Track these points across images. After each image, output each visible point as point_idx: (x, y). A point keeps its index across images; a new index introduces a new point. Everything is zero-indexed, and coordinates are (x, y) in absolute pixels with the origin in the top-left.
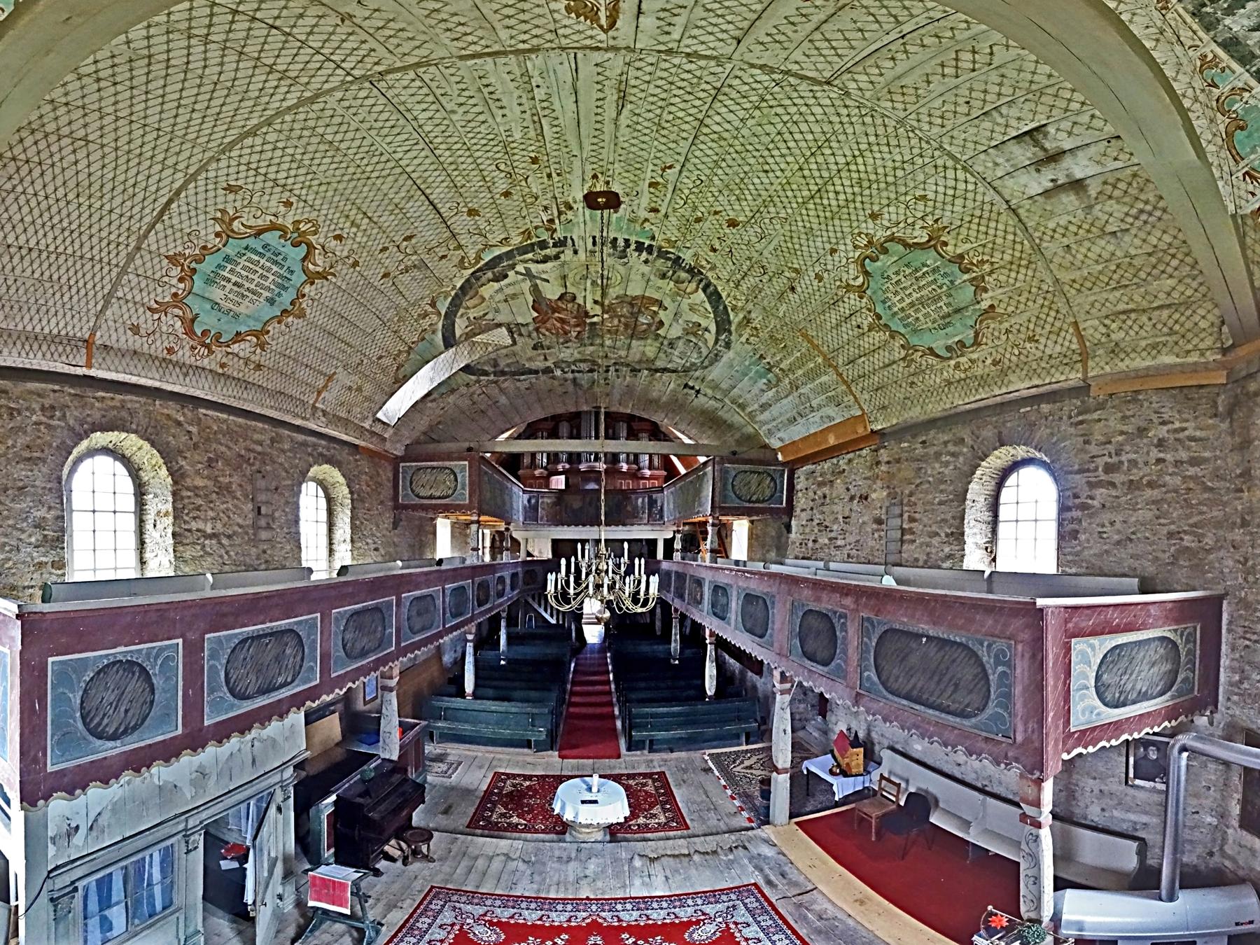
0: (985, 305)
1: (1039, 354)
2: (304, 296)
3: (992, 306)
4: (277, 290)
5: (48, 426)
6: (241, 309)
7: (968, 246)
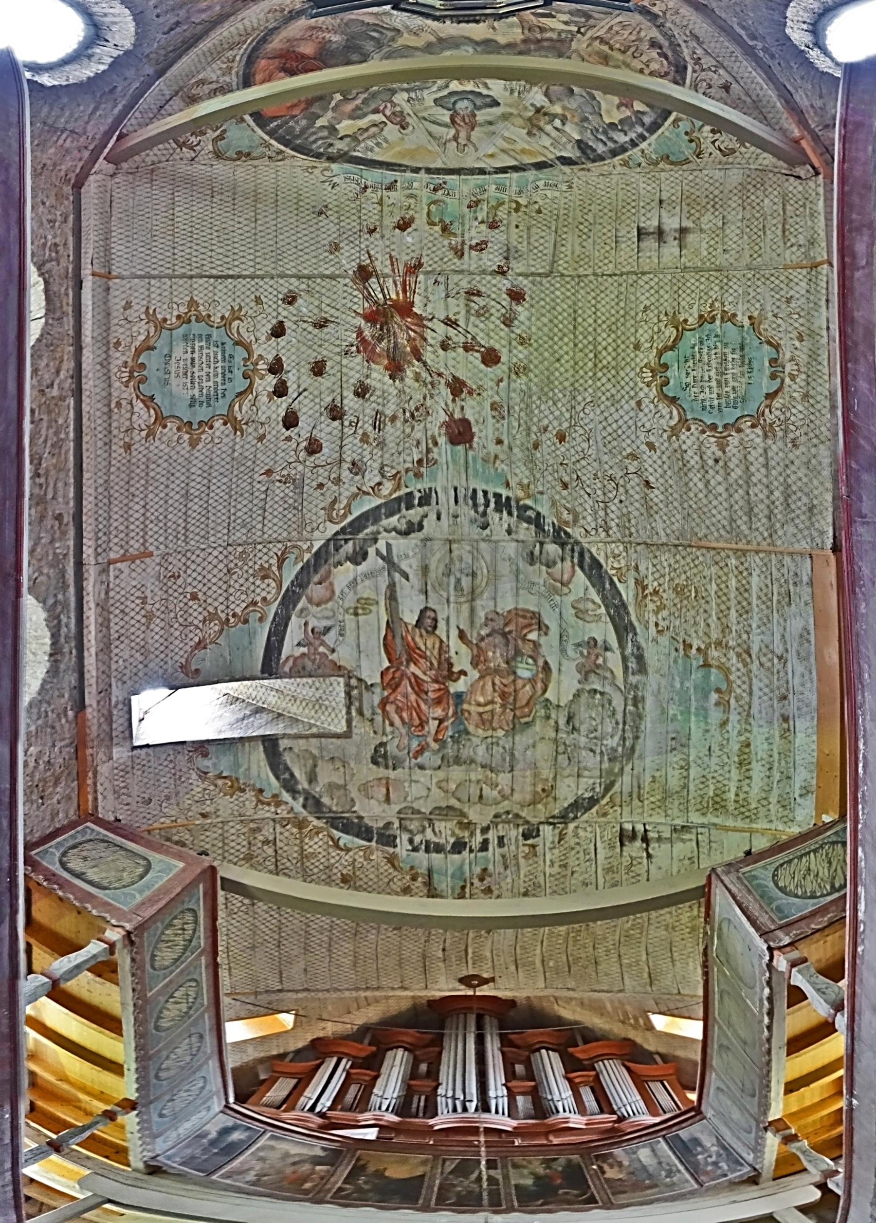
0: (746, 322)
1: (803, 300)
2: (211, 427)
3: (750, 318)
4: (204, 398)
5: (44, 245)
6: (174, 381)
7: (696, 307)
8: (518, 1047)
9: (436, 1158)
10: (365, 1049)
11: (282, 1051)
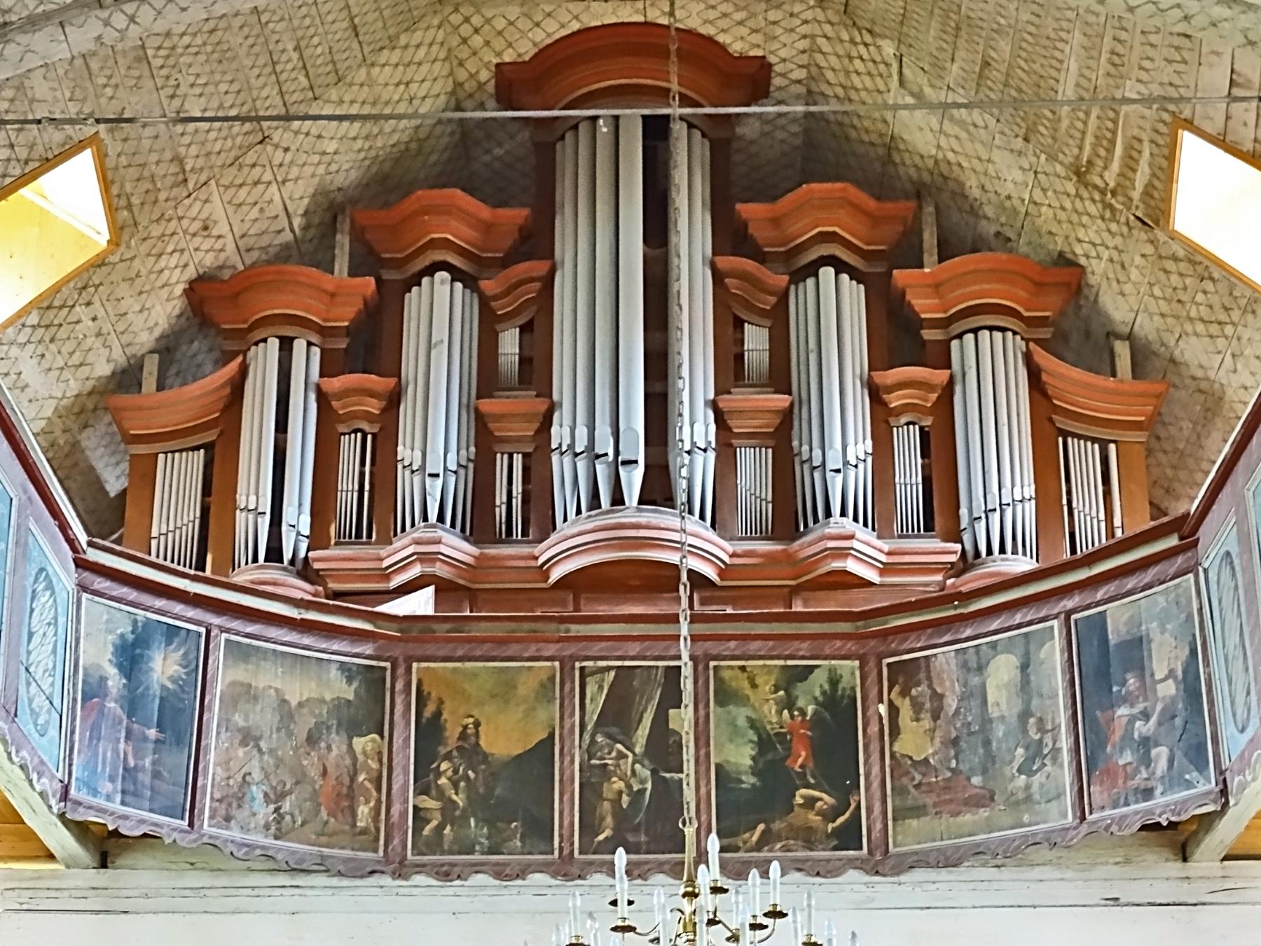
8: (760, 257)
9: (566, 663)
10: (344, 290)
11: (119, 357)
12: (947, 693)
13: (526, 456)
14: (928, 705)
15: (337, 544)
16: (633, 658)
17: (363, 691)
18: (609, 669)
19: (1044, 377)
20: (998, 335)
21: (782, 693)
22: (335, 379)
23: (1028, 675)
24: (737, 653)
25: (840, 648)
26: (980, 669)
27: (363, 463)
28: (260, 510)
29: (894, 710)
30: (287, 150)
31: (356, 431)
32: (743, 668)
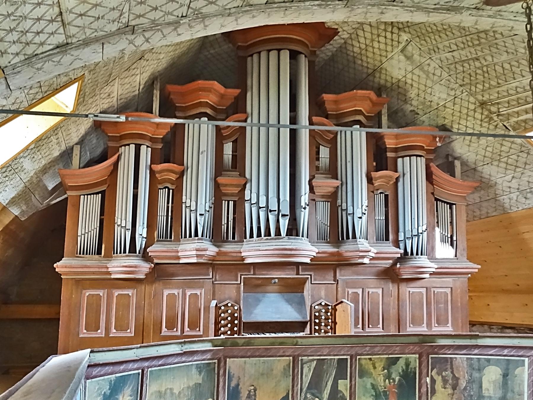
12: (461, 378)
13: (235, 202)
14: (450, 381)
15: (157, 241)
16: (325, 356)
17: (206, 379)
18: (315, 360)
19: (434, 177)
20: (419, 158)
21: (386, 371)
22: (159, 166)
23: (507, 380)
24: (369, 352)
25: (411, 350)
26: (480, 370)
27: (168, 203)
28: (127, 228)
29: (433, 381)
30: (148, 60)
31: (165, 188)
32: (370, 359)
